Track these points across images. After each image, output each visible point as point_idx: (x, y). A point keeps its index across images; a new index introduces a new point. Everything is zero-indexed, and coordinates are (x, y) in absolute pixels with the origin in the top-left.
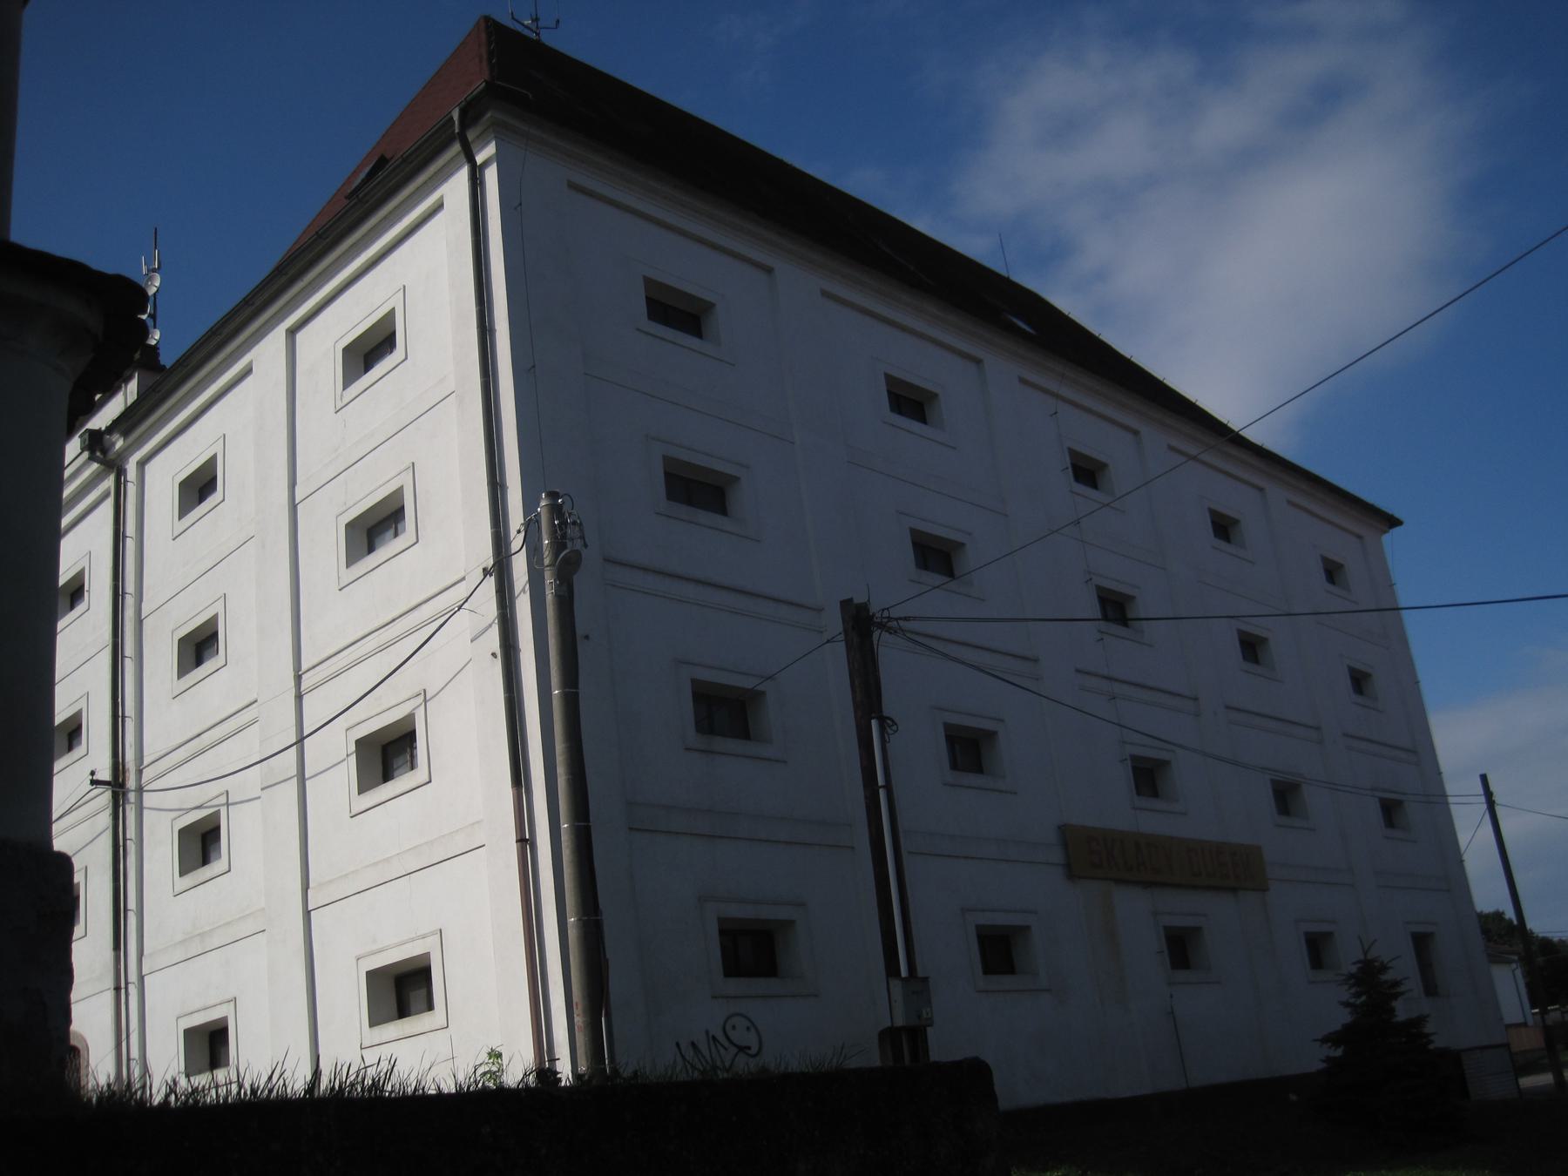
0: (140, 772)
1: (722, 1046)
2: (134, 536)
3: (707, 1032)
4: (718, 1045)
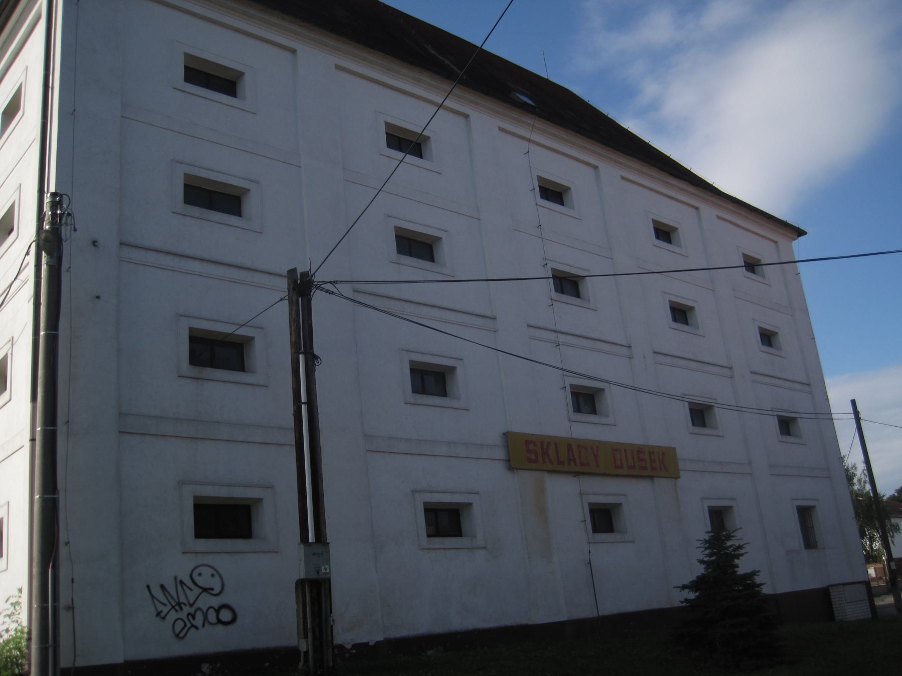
3: (176, 578)
4: (185, 588)
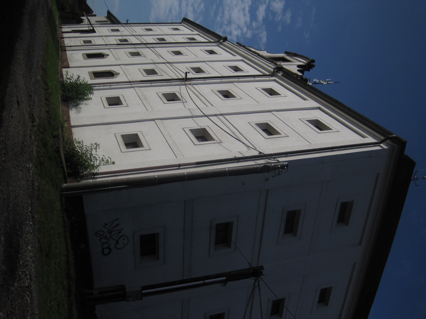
0: (190, 84)
1: (118, 235)
3: (122, 230)
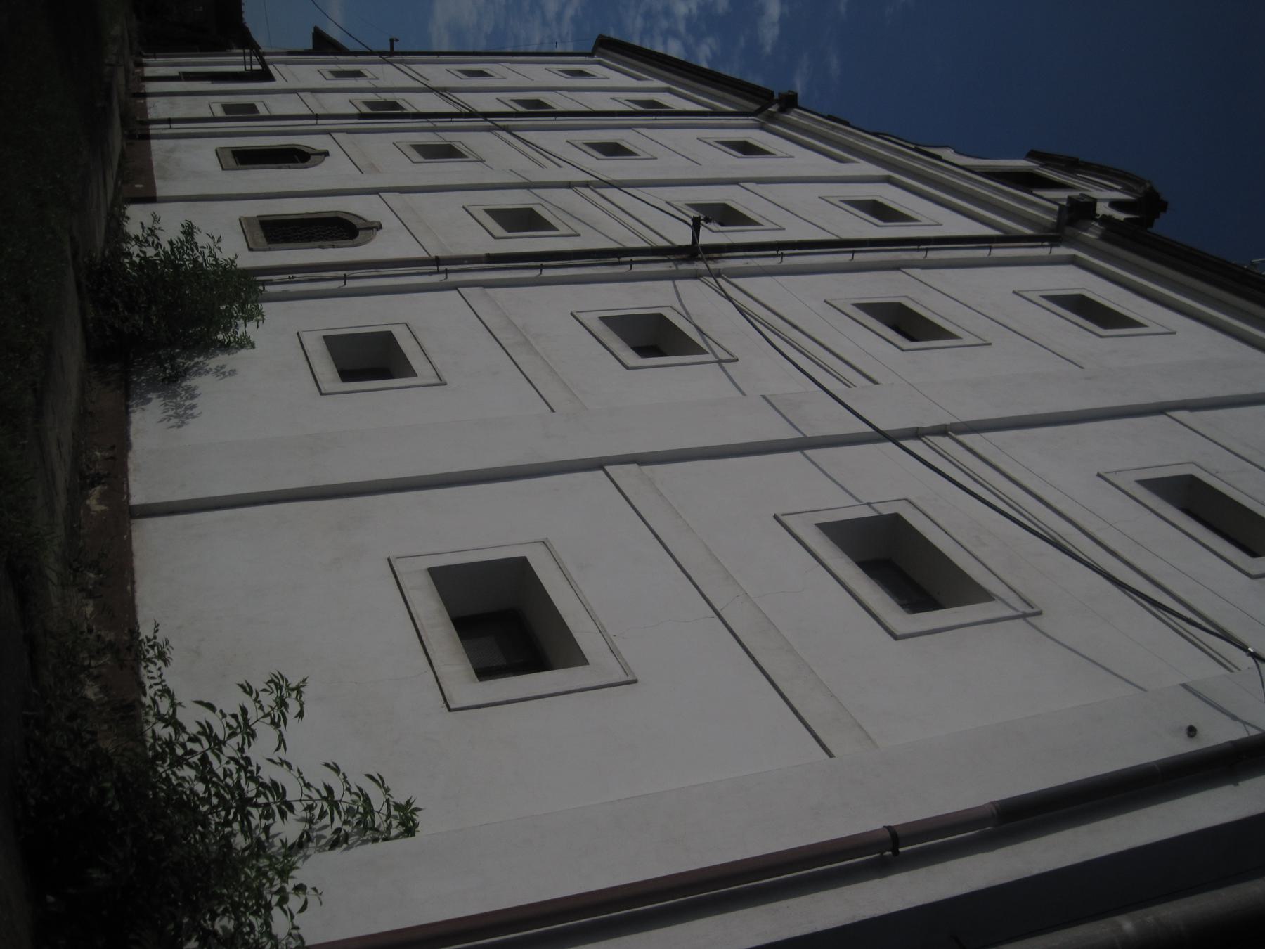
2: (1052, 254)
